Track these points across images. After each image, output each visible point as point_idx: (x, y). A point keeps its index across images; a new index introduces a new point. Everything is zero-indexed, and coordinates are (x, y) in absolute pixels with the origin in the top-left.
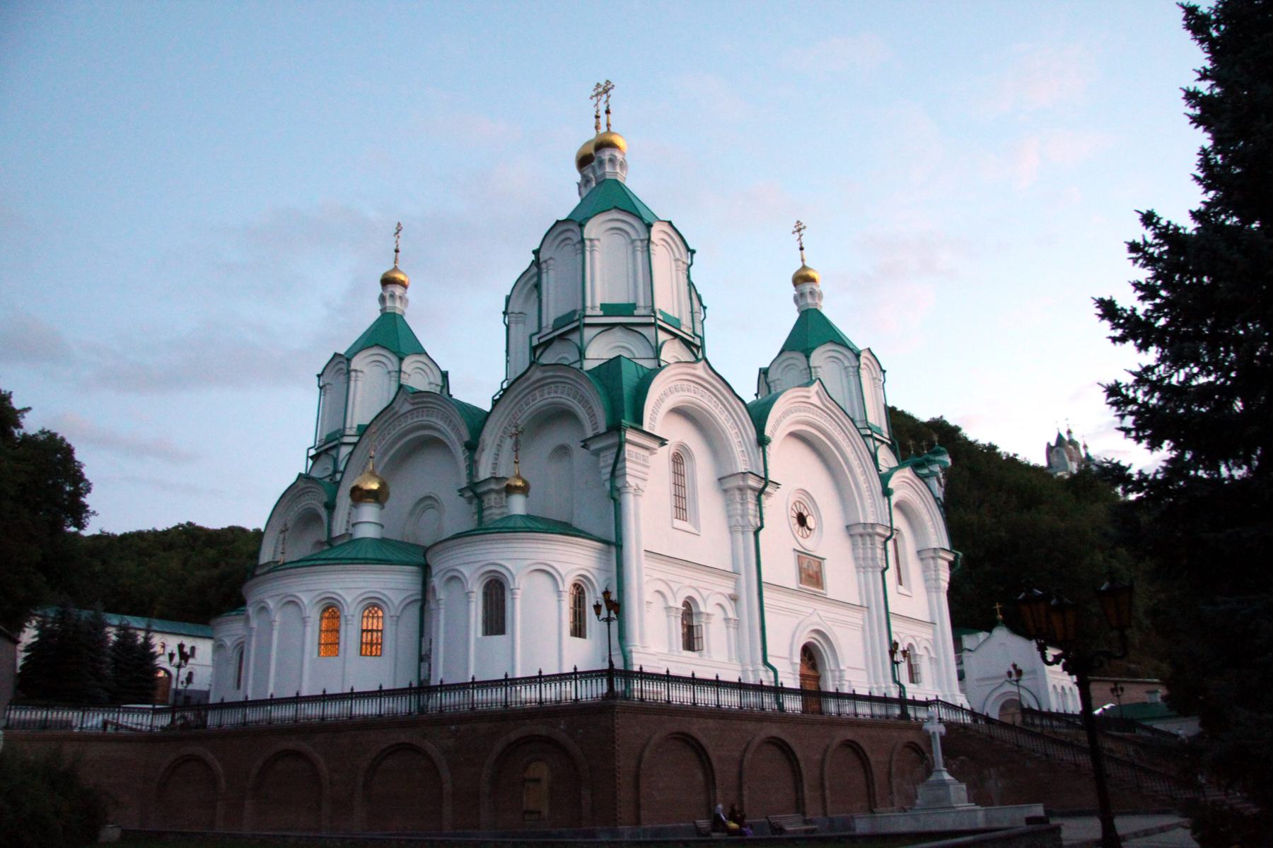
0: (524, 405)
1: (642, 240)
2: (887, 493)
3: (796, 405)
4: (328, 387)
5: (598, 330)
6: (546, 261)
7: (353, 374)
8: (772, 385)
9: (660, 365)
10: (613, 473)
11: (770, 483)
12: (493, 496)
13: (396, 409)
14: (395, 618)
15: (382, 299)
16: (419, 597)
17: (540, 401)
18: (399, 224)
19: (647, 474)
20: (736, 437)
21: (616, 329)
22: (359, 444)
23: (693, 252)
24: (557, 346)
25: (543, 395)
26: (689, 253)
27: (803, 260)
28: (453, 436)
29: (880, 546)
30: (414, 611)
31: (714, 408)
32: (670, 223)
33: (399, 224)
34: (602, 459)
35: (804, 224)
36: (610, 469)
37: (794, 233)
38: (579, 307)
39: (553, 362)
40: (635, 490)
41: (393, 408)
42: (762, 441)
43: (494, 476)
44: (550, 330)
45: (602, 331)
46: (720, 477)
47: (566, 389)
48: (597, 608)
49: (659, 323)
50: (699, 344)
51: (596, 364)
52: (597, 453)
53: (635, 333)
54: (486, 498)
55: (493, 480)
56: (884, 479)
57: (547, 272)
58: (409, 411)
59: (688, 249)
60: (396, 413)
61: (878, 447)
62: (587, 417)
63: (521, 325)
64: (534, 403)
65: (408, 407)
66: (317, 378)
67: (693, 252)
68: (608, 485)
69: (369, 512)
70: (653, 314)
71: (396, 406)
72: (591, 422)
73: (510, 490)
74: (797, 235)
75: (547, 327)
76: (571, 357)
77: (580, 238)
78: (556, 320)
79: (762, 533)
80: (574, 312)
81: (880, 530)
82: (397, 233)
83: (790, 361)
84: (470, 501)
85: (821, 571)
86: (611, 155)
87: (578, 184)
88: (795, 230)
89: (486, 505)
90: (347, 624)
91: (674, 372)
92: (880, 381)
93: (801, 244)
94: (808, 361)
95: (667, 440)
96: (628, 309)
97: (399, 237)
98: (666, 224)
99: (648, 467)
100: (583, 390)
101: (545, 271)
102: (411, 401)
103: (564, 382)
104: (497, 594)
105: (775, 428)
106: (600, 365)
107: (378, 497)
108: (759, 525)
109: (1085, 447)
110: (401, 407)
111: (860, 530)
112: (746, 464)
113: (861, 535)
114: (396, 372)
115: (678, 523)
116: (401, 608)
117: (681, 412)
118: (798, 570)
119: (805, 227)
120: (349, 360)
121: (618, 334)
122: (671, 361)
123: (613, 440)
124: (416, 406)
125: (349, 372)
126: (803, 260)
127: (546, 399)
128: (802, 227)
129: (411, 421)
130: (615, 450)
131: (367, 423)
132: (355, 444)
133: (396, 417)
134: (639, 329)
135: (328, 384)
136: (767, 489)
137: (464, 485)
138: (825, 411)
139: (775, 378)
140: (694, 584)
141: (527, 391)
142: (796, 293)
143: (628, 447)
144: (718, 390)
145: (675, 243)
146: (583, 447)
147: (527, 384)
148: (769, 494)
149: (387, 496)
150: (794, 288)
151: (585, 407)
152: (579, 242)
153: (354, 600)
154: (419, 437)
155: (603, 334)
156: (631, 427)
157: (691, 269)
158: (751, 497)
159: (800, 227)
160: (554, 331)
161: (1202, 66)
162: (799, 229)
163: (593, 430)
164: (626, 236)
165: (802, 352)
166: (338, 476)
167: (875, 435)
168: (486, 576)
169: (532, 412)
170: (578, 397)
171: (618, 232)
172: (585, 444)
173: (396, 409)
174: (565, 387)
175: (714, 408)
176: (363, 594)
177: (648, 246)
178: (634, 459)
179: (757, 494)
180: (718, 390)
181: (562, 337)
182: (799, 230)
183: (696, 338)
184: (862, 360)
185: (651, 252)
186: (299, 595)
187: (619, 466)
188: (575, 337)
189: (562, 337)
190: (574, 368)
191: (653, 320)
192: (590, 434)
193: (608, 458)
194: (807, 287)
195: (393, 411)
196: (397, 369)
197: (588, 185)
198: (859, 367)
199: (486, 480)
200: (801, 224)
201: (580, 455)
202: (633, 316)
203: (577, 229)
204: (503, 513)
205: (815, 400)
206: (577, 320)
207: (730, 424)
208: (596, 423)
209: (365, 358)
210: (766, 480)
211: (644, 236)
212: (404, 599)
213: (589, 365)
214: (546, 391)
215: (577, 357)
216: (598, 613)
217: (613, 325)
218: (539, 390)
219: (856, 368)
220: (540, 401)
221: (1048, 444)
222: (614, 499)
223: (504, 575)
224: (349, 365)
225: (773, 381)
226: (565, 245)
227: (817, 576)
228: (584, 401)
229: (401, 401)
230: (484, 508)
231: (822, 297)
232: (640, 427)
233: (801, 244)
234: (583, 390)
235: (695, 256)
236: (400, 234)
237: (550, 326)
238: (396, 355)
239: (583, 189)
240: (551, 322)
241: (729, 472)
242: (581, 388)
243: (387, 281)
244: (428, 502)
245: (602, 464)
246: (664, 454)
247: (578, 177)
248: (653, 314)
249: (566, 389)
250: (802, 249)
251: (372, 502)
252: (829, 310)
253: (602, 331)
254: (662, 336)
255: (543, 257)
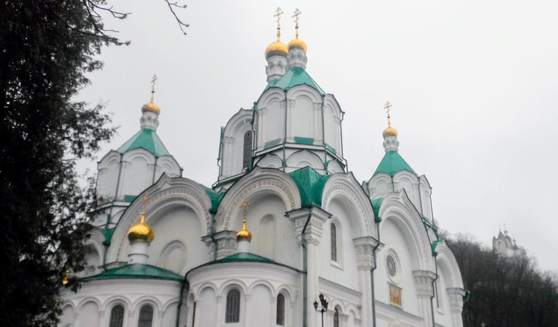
0: (248, 190)
1: (318, 104)
2: (435, 254)
3: (393, 202)
4: (104, 170)
5: (293, 151)
6: (261, 110)
7: (123, 163)
8: (370, 190)
9: (327, 174)
10: (303, 232)
11: (380, 244)
12: (224, 242)
13: (159, 187)
14: (161, 313)
15: (143, 120)
16: (178, 300)
17: (258, 189)
18: (155, 76)
19: (321, 233)
20: (364, 217)
21: (304, 152)
22: (130, 207)
23: (343, 113)
24: (268, 157)
25: (261, 185)
26: (341, 114)
27: (389, 124)
28: (198, 204)
29: (430, 283)
30: (174, 308)
31: (354, 200)
32: (333, 95)
33: (155, 76)
34: (296, 223)
35: (391, 104)
36: (302, 229)
37: (385, 108)
38: (282, 137)
39: (265, 167)
40: (315, 242)
41: (157, 186)
42: (377, 220)
43: (226, 229)
44: (262, 149)
45: (297, 152)
46: (354, 238)
47: (275, 183)
48: (316, 304)
49: (327, 150)
50: (345, 164)
51: (293, 170)
52: (294, 220)
53: (315, 155)
54: (219, 243)
55: (226, 232)
56: (433, 247)
57: (262, 116)
58: (167, 189)
59: (341, 111)
60: (159, 189)
61: (428, 229)
62: (288, 199)
63: (231, 145)
64: (254, 189)
65: (167, 186)
66: (97, 164)
67: (343, 113)
68: (300, 238)
69: (139, 248)
70: (324, 146)
71: (159, 185)
72: (291, 202)
73: (240, 238)
74: (386, 109)
75: (261, 147)
76: (277, 165)
77: (284, 99)
78: (266, 144)
79: (375, 271)
80: (279, 140)
81: (431, 275)
82: (154, 81)
83: (384, 179)
84: (208, 244)
85: (400, 295)
86: (299, 53)
87: (266, 67)
88: (294, 15)
89: (219, 247)
90: (245, 301)
91: (336, 178)
92: (429, 193)
93: (388, 115)
94: (392, 179)
95: (332, 215)
96: (310, 141)
97: (154, 84)
98: (331, 96)
99: (322, 229)
100: (286, 183)
101: (261, 115)
102: (172, 183)
103: (275, 179)
104: (235, 299)
105: (382, 214)
106: (295, 171)
107: (146, 239)
108: (374, 266)
109: (514, 241)
110: (163, 186)
111: (420, 274)
112: (368, 232)
113: (420, 277)
114: (152, 165)
115: (333, 263)
116: (165, 307)
117: (336, 201)
118: (389, 294)
119: (391, 106)
120: (122, 155)
121: (305, 154)
122: (333, 172)
123: (306, 212)
124: (173, 186)
125: (121, 162)
126: (389, 124)
127: (262, 187)
128: (389, 105)
129: (168, 195)
130: (306, 219)
131: (137, 194)
132: (128, 207)
133: (158, 191)
134: (314, 152)
135: (105, 168)
136: (379, 247)
137: (205, 233)
138: (405, 207)
139: (373, 187)
140: (341, 298)
141: (251, 182)
142: (384, 141)
143: (312, 218)
144: (355, 188)
145: (334, 105)
146: (285, 216)
147: (251, 178)
148: (379, 250)
149: (152, 238)
150: (383, 139)
151: (287, 194)
152: (283, 101)
153: (105, 302)
154: (174, 204)
155: (296, 153)
156: (316, 207)
157: (342, 122)
158: (370, 250)
159: (388, 105)
160: (265, 150)
161: (294, 22)
162: (388, 106)
163: (292, 207)
164: (307, 98)
165: (389, 174)
166: (111, 226)
167: (427, 223)
168: (231, 287)
169: (252, 195)
170: (283, 187)
171: (304, 97)
172: (287, 214)
173: (159, 187)
174: (275, 181)
175: (354, 200)
176: (141, 298)
177: (322, 108)
178: (315, 224)
179: (373, 249)
180: (355, 188)
181: (271, 153)
182: (388, 107)
183: (343, 160)
184: (421, 181)
185: (324, 111)
186: (98, 297)
187: (308, 227)
188: (280, 154)
189: (271, 153)
190: (281, 171)
191: (323, 149)
192: (289, 209)
193: (301, 223)
194: (390, 139)
195: (157, 188)
196: (154, 163)
197: (272, 68)
198: (419, 185)
199: (222, 232)
200: (389, 104)
201: (281, 222)
202: (312, 145)
203: (282, 93)
204: (230, 252)
205: (401, 201)
206: (282, 144)
207: (361, 209)
208: (294, 203)
209: (132, 155)
210: (379, 243)
211: (320, 101)
212: (170, 300)
213: (288, 170)
214: (262, 183)
215: (281, 166)
216: (316, 307)
217: (302, 150)
218: (258, 182)
219: (417, 185)
220: (258, 189)
221: (494, 238)
222: (304, 247)
223: (239, 286)
224: (122, 158)
225: (372, 189)
226: (274, 101)
227: (399, 299)
228: (285, 189)
229: (163, 182)
230: (218, 248)
231: (399, 145)
232: (320, 206)
233: (388, 115)
234: (286, 183)
235: (345, 115)
236: (156, 81)
237: (263, 147)
238: (153, 155)
239: (269, 70)
240: (264, 144)
241: (359, 236)
242: (285, 182)
243: (145, 110)
244: (176, 243)
245: (296, 226)
246: (328, 222)
247: (266, 63)
248: (324, 146)
249: (275, 183)
250: (389, 117)
251: (142, 242)
252: (402, 152)
253: (297, 152)
254: (329, 158)
255: (260, 106)
